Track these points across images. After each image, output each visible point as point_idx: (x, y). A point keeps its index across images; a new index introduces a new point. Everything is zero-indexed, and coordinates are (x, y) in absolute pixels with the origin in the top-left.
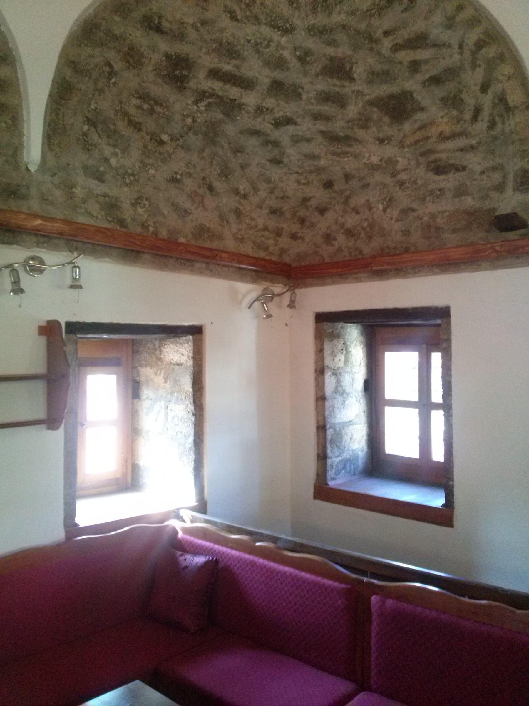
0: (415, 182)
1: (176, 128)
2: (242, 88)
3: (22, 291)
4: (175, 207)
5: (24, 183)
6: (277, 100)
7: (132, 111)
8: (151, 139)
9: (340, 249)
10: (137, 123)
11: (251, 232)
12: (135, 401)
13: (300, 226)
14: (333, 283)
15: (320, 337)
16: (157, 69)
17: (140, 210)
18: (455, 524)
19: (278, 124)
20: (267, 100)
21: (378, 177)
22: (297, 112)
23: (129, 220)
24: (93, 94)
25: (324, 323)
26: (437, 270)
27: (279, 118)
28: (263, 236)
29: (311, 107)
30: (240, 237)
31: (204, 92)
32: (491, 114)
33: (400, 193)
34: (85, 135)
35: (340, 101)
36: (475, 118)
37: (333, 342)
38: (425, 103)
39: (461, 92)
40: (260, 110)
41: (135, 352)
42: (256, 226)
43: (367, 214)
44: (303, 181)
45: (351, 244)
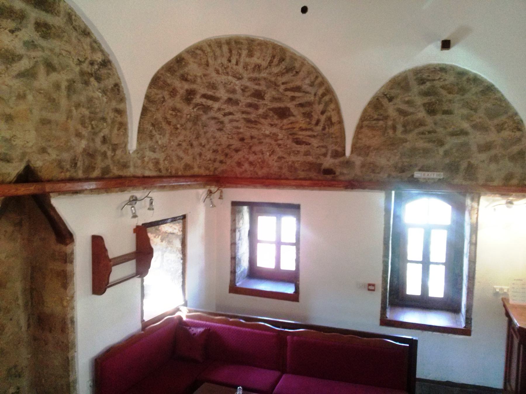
0: (286, 146)
7: (169, 116)
13: (224, 157)
19: (225, 115)
21: (268, 140)
32: (324, 124)
33: (278, 149)
35: (256, 107)
36: (317, 124)
39: (312, 112)
40: (219, 109)
43: (261, 156)
45: (252, 169)
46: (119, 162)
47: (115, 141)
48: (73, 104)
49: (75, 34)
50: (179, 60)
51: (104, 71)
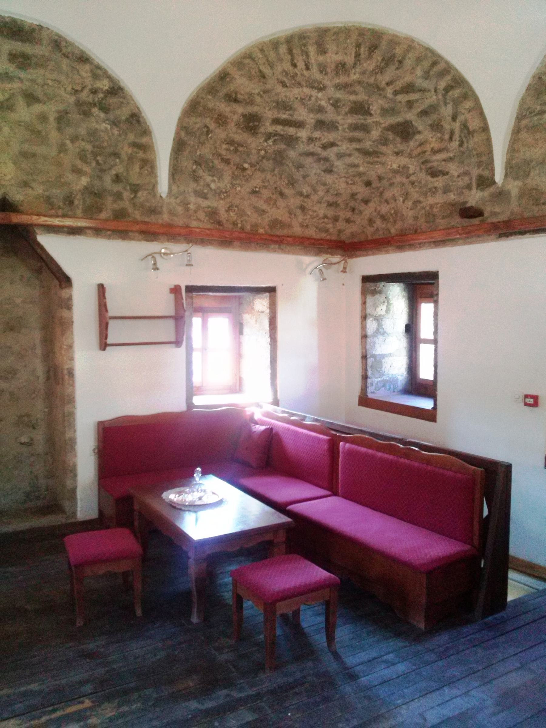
0: (420, 182)
1: (254, 158)
2: (297, 127)
3: (158, 269)
4: (256, 209)
5: (160, 205)
6: (321, 132)
7: (224, 153)
8: (237, 168)
9: (377, 229)
10: (227, 160)
11: (314, 220)
12: (241, 336)
13: (351, 213)
14: (373, 254)
15: (364, 293)
16: (237, 125)
17: (232, 214)
18: (438, 420)
19: (325, 147)
20: (315, 133)
21: (399, 179)
22: (337, 138)
23: (225, 222)
24: (198, 146)
25: (367, 283)
26: (433, 245)
27: (325, 143)
28: (323, 222)
29: (346, 134)
30: (305, 225)
31: (271, 133)
32: (460, 136)
33: (412, 190)
34: (194, 171)
36: (451, 138)
37: (375, 297)
38: (421, 128)
39: (440, 120)
40: (311, 140)
41: (240, 304)
42: (317, 216)
44: (350, 182)
45: (384, 226)
46: (142, 206)
47: (135, 179)
48: (68, 137)
49: (65, 61)
50: (223, 76)
51: (113, 101)
